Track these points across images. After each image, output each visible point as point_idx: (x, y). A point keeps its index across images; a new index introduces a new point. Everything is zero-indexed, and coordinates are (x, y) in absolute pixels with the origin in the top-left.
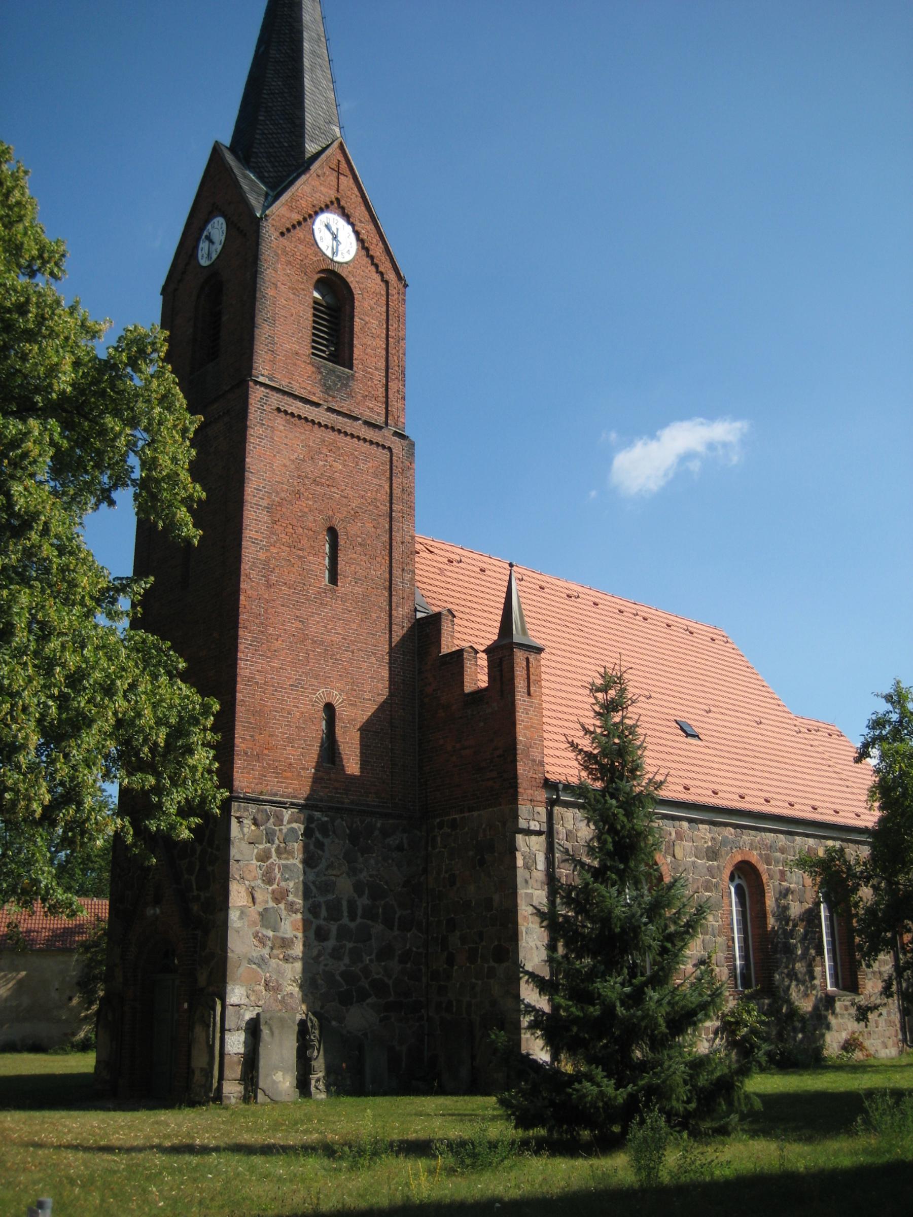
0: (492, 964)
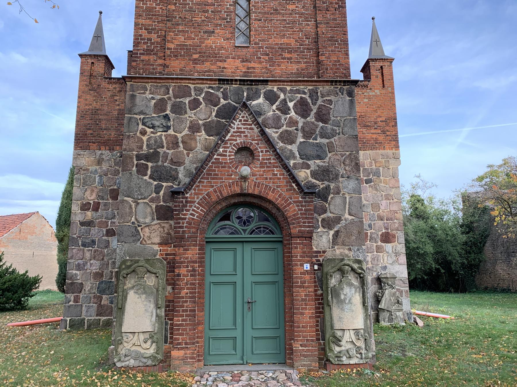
0: (380, 243)
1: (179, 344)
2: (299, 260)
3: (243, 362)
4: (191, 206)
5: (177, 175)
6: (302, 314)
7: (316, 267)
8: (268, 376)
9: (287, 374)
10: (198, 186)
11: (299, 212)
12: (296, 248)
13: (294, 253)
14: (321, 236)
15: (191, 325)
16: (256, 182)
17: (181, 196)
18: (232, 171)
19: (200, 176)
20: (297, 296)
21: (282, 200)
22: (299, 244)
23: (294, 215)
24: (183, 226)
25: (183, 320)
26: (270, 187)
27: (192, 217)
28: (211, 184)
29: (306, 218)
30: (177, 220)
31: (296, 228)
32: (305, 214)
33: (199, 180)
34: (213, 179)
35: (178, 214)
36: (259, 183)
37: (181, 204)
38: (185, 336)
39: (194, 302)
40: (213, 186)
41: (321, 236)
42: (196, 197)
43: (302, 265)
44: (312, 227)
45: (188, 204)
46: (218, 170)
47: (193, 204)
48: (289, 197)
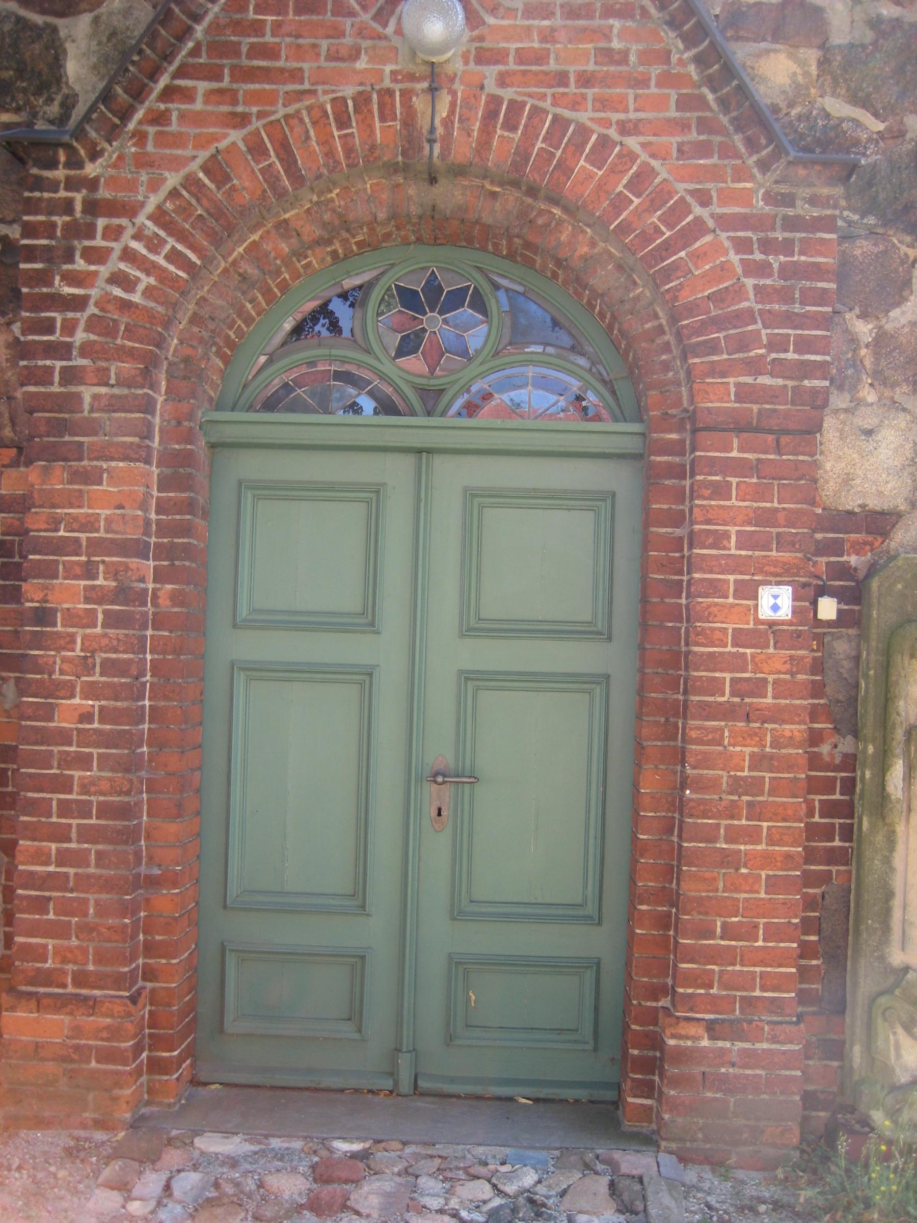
1: (47, 978)
2: (737, 566)
3: (396, 1083)
4: (113, 233)
5: (57, 63)
6: (729, 860)
7: (828, 608)
8: (510, 1189)
9: (623, 1184)
10: (159, 118)
11: (749, 282)
12: (721, 491)
13: (708, 522)
14: (869, 433)
15: (107, 885)
16: (495, 101)
17: (60, 174)
18: (361, 32)
19: (168, 57)
20: (705, 761)
21: (653, 205)
22: (740, 468)
23: (718, 298)
24: (69, 346)
25: (63, 858)
26: (583, 132)
27: (118, 292)
28: (235, 102)
29: (790, 319)
30: (35, 309)
31: (723, 375)
32: (785, 296)
33: (163, 81)
34: (250, 75)
35: (44, 278)
36: (515, 107)
37: (59, 220)
38: (74, 942)
39: (129, 766)
40: (242, 120)
41: (869, 433)
42: (144, 177)
43: (749, 591)
44: (821, 369)
45: (101, 223)
46: (277, 26)
47: (124, 221)
48: (692, 193)
